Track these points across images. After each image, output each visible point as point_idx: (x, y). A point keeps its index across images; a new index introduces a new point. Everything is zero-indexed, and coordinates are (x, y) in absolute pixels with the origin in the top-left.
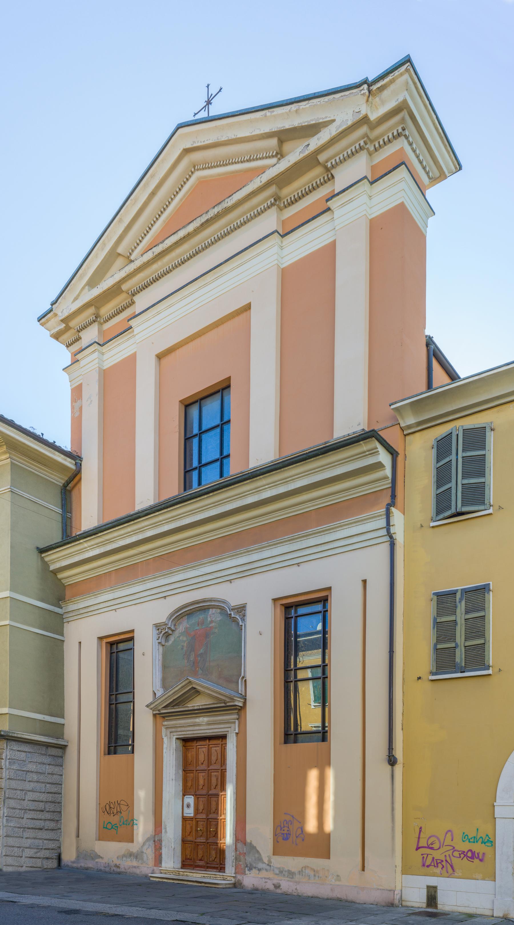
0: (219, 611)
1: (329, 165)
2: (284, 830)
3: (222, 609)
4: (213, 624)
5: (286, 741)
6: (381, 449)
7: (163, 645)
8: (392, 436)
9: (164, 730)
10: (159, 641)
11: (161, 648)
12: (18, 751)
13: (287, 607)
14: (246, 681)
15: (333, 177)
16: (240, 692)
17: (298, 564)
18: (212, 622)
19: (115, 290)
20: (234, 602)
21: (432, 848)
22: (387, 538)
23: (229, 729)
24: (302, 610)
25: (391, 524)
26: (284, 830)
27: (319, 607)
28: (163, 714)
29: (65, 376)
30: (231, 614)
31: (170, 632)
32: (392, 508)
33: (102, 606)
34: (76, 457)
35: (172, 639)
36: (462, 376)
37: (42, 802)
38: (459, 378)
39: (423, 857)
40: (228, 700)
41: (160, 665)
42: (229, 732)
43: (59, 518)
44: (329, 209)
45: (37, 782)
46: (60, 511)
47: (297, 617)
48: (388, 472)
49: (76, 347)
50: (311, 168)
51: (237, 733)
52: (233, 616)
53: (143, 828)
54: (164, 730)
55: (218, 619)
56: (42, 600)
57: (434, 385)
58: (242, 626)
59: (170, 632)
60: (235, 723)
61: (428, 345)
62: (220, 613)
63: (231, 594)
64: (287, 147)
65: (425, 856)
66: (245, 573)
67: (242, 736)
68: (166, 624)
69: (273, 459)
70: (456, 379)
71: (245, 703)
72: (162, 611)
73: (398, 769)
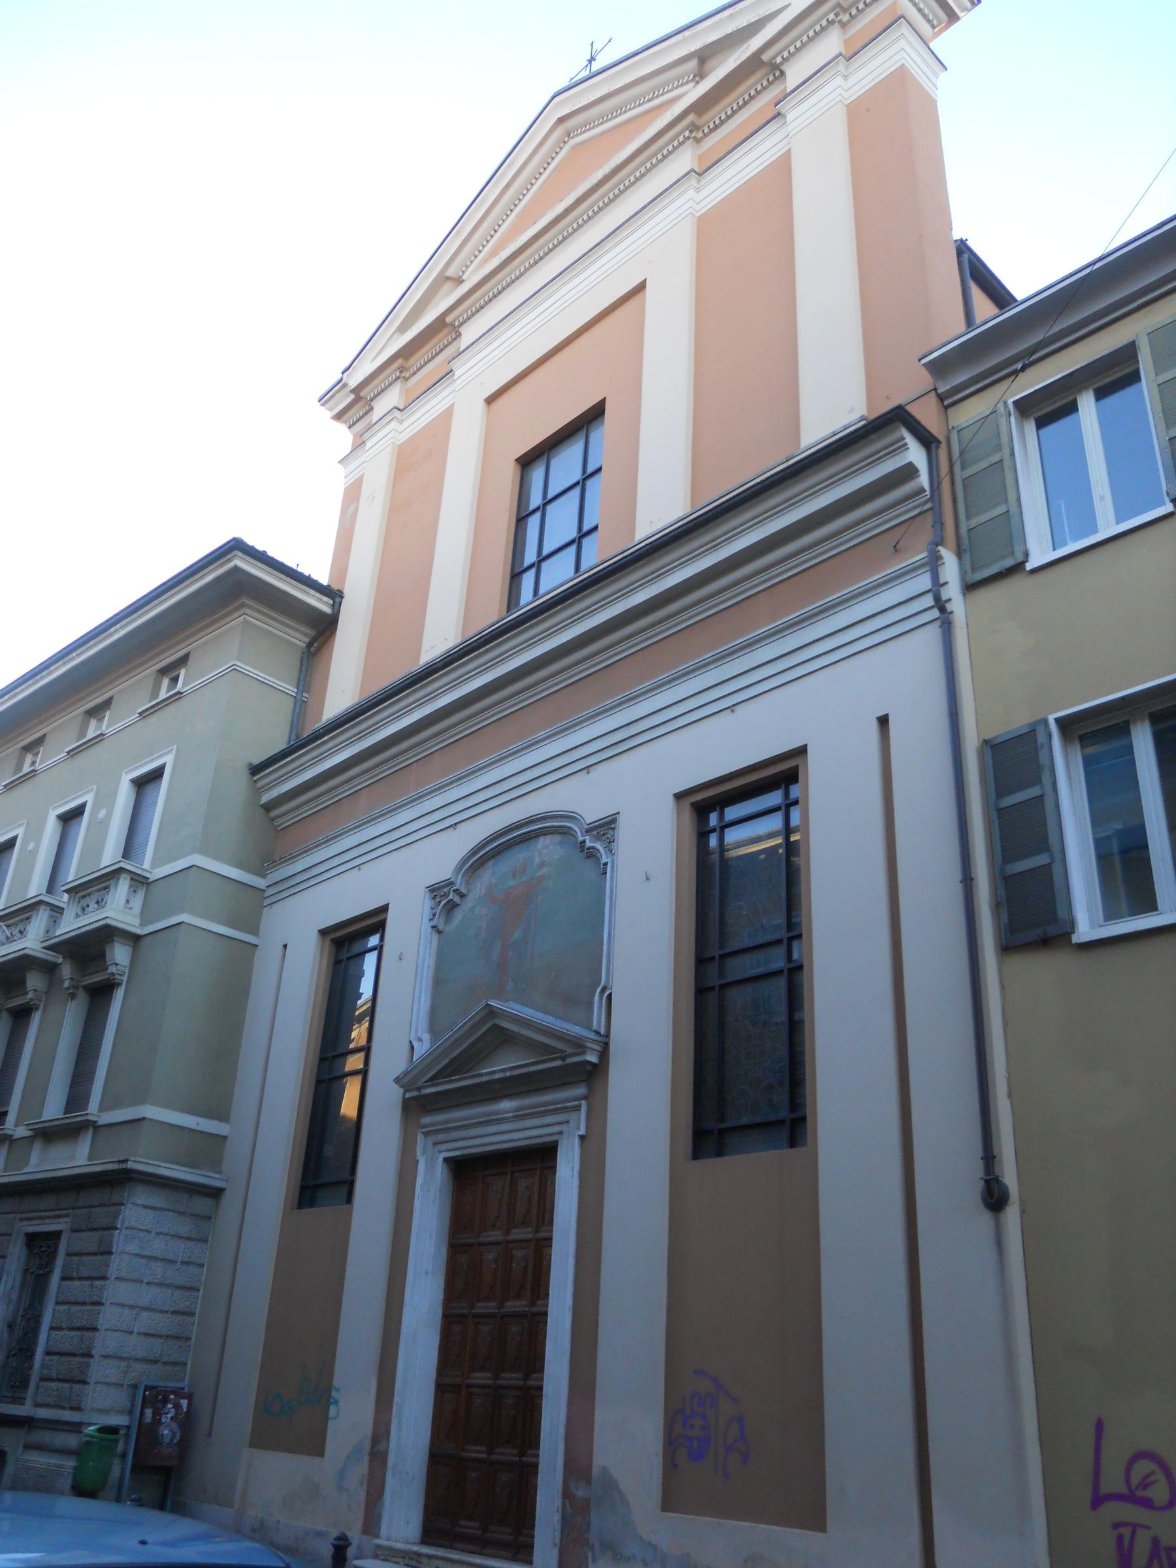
0: (557, 838)
1: (779, 60)
2: (692, 1426)
3: (565, 832)
4: (545, 870)
5: (698, 1152)
6: (910, 440)
7: (439, 932)
8: (927, 414)
9: (420, 1138)
10: (434, 923)
11: (435, 938)
12: (146, 1207)
13: (702, 810)
14: (610, 996)
15: (782, 73)
16: (595, 1027)
17: (731, 708)
18: (542, 864)
19: (439, 324)
20: (592, 814)
21: (1147, 1503)
22: (935, 613)
23: (564, 1128)
24: (732, 813)
25: (942, 581)
26: (692, 1426)
27: (774, 798)
28: (421, 1102)
29: (341, 471)
30: (584, 842)
31: (457, 899)
32: (940, 548)
33: (379, 842)
34: (334, 594)
35: (458, 915)
36: (1019, 297)
37: (159, 1336)
38: (1015, 300)
39: (1120, 1539)
40: (569, 1050)
41: (430, 980)
42: (565, 1135)
43: (289, 704)
44: (779, 114)
45: (161, 1285)
46: (292, 690)
47: (723, 828)
48: (924, 479)
49: (360, 426)
50: (752, 72)
51: (582, 1138)
52: (588, 844)
53: (350, 1417)
54: (420, 1138)
55: (556, 857)
56: (240, 865)
57: (978, 321)
58: (605, 864)
59: (457, 899)
60: (578, 1108)
61: (960, 253)
62: (561, 843)
63: (583, 798)
64: (709, 65)
65: (1126, 1532)
66: (620, 747)
67: (593, 1146)
68: (452, 883)
69: (679, 514)
70: (1008, 304)
71: (604, 1053)
72: (442, 856)
73: (1012, 1215)
